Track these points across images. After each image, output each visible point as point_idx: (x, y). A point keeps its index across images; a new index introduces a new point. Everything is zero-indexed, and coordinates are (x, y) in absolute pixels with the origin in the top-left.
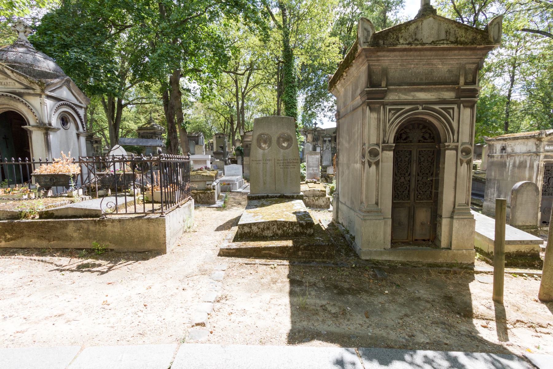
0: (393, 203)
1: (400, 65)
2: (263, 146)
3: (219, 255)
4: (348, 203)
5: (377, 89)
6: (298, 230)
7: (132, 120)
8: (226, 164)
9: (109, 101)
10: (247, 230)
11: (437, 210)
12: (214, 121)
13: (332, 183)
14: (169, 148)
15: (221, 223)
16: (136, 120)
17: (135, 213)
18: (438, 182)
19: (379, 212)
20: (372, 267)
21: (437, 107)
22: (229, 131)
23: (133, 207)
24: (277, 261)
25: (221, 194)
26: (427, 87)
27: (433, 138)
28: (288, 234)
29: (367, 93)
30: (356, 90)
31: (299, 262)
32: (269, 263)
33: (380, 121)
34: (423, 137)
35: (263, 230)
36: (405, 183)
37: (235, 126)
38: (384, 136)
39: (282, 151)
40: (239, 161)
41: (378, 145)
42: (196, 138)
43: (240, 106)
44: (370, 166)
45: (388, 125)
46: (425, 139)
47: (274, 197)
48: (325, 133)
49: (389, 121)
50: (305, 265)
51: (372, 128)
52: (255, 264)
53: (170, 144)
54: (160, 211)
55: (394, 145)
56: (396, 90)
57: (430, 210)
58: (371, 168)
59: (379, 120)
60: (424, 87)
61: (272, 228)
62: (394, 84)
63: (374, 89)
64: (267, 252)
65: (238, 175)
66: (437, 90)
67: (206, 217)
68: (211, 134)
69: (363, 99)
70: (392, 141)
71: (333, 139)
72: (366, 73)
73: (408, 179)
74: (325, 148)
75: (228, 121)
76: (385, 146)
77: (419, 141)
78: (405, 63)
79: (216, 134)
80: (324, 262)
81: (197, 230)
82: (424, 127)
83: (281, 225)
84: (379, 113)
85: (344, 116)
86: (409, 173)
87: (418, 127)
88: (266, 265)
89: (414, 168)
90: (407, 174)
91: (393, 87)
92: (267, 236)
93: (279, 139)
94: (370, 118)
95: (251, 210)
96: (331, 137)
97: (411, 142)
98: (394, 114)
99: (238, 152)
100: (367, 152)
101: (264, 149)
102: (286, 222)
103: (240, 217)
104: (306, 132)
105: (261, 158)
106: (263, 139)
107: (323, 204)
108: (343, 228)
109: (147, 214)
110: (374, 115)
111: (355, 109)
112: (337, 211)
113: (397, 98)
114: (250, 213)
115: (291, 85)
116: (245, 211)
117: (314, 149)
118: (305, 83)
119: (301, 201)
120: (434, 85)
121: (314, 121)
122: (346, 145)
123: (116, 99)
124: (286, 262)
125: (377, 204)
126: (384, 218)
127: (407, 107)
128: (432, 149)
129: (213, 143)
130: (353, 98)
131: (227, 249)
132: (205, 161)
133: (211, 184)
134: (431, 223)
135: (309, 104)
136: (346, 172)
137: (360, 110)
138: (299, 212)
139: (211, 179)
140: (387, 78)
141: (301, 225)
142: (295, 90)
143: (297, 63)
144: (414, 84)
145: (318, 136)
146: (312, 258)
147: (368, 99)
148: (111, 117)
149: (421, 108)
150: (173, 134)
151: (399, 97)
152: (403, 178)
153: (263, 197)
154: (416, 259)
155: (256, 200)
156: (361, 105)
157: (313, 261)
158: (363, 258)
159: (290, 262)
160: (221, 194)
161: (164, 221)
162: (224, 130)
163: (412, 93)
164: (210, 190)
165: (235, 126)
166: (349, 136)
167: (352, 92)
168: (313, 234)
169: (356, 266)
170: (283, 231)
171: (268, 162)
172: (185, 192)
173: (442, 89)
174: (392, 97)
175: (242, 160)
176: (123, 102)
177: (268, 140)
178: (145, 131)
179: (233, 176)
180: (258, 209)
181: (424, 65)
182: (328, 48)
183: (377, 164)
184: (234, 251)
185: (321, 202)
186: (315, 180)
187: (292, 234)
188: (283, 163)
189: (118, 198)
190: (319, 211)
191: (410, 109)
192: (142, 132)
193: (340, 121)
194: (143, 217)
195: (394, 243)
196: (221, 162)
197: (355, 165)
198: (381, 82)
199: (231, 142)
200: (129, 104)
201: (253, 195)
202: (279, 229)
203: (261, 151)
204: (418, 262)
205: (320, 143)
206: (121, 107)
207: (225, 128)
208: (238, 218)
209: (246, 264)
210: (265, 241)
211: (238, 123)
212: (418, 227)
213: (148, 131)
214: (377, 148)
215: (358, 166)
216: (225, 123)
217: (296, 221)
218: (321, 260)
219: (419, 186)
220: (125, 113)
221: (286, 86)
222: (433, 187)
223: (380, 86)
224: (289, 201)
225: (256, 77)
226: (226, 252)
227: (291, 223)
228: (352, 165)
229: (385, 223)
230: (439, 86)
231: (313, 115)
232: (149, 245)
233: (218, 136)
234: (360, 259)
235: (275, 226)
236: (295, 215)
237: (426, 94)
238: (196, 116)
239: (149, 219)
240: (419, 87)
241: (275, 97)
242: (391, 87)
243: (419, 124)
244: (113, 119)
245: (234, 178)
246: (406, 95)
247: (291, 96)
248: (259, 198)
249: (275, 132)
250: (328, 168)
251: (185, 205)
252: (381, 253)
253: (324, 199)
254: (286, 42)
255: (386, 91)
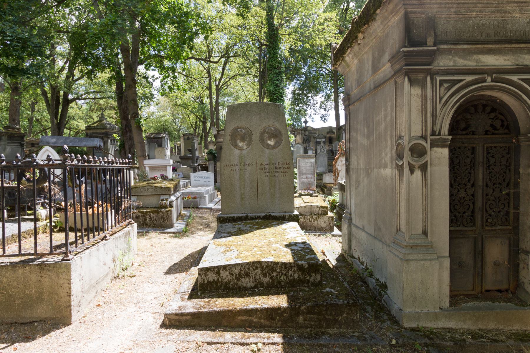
0: (450, 231)
1: (455, 13)
2: (240, 144)
3: (164, 325)
4: (370, 229)
5: (421, 48)
6: (296, 276)
7: (82, 119)
8: (195, 171)
9: (52, 96)
10: (212, 277)
11: (518, 241)
12: (183, 121)
13: (331, 194)
14: (123, 151)
15: (177, 259)
16: (87, 117)
17: (20, 254)
18: (519, 197)
19: (430, 247)
20: (426, 345)
21: (515, 78)
22: (201, 132)
23: (33, 239)
24: (263, 334)
25: (183, 212)
26: (497, 46)
27: (507, 127)
28: (279, 282)
29: (405, 56)
30: (381, 56)
31: (300, 336)
32: (248, 341)
33: (426, 99)
34: (492, 125)
35: (239, 277)
36: (467, 198)
37: (208, 124)
38: (434, 123)
39: (267, 151)
40: (211, 167)
41: (424, 137)
42: (159, 140)
43: (214, 101)
44: (412, 171)
45: (439, 107)
46: (495, 128)
47: (256, 219)
48: (317, 132)
49: (441, 99)
50: (310, 342)
51: (412, 111)
52: (223, 343)
53: (124, 147)
54: (64, 249)
55: (450, 137)
56: (449, 52)
57: (507, 242)
58: (414, 175)
59: (424, 98)
60: (493, 46)
61: (254, 273)
62: (446, 43)
63: (416, 49)
64: (245, 318)
65: (208, 186)
66: (513, 51)
67: (155, 249)
68: (179, 136)
69: (397, 67)
70: (447, 132)
71: (327, 140)
72: (402, 26)
73: (470, 192)
74: (318, 151)
75: (200, 121)
76: (436, 139)
77: (486, 133)
78: (462, 10)
79: (184, 135)
80: (342, 335)
81: (137, 273)
82: (493, 110)
83: (268, 268)
84: (423, 86)
85: (359, 100)
86: (472, 182)
87: (484, 111)
88: (243, 344)
89: (480, 174)
90: (469, 185)
91: (445, 47)
92: (244, 287)
93: (262, 134)
94: (410, 95)
95: (220, 240)
96: (325, 137)
97: (473, 133)
98: (449, 89)
99: (210, 156)
100: (407, 150)
101: (241, 149)
102: (276, 264)
103: (206, 248)
104: (295, 131)
105: (237, 162)
106: (241, 135)
107: (324, 225)
108: (362, 266)
109: (42, 255)
110: (417, 91)
111: (378, 86)
112: (349, 239)
113: (451, 63)
114: (220, 245)
115: (277, 71)
116: (212, 242)
117: (306, 152)
118: (293, 73)
119: (296, 224)
120: (508, 44)
121: (303, 120)
122: (363, 141)
123: (62, 93)
124: (277, 338)
125: (425, 233)
126: (438, 257)
127: (469, 78)
128: (508, 145)
129: (180, 146)
130: (375, 69)
131: (176, 314)
132: (165, 168)
133: (167, 199)
134: (509, 263)
135: (297, 99)
136: (365, 181)
137: (390, 87)
138: (296, 244)
139: (167, 191)
140: (435, 33)
141: (301, 268)
142: (281, 77)
143: (284, 47)
144: (477, 42)
145: (309, 136)
146: (321, 327)
147: (406, 65)
148: (54, 115)
149: (489, 79)
150: (129, 134)
151: (454, 62)
152: (462, 191)
153: (240, 219)
154: (492, 326)
155: (232, 223)
156: (393, 76)
157: (323, 334)
158: (407, 325)
159: (284, 338)
160: (183, 212)
161: (68, 268)
162: (195, 130)
163: (475, 57)
164: (166, 207)
165: (208, 124)
166: (368, 127)
167: (373, 62)
168: (320, 282)
169: (397, 342)
170: (272, 277)
171: (247, 167)
172: (123, 215)
173: (521, 51)
174: (444, 62)
175: (215, 167)
176: (70, 97)
177: (247, 137)
178: (95, 131)
179: (202, 186)
180: (232, 238)
181: (492, 12)
182: (322, 27)
183: (424, 168)
184: (189, 317)
185: (322, 222)
186: (311, 192)
187: (286, 283)
188: (269, 169)
189: (6, 224)
190: (319, 236)
191: (472, 81)
192: (90, 132)
193: (351, 107)
194: (33, 260)
195: (455, 297)
196: (189, 168)
197: (382, 170)
198: (426, 38)
199: (203, 145)
200: (78, 98)
201: (226, 216)
202: (265, 275)
203: (237, 152)
204: (497, 331)
205: (312, 144)
206: (67, 102)
207: (196, 128)
208: (201, 252)
209: (208, 343)
210: (242, 296)
211: (212, 122)
212: (489, 269)
213: (98, 131)
214: (423, 142)
215: (388, 172)
216: (196, 122)
217: (292, 261)
218: (336, 331)
219: (489, 203)
220: (73, 110)
221: (271, 71)
222: (512, 205)
223: (424, 44)
224: (278, 225)
225: (235, 64)
226: (175, 320)
227: (285, 265)
228: (376, 170)
229: (441, 265)
230: (517, 46)
231: (301, 113)
232: (42, 311)
233: (186, 137)
234: (402, 327)
235: (259, 271)
236: (289, 250)
237: (497, 57)
238: (162, 114)
239: (42, 265)
240: (486, 46)
241: (256, 91)
242: (442, 47)
243: (484, 106)
244: (56, 117)
245: (203, 190)
246: (466, 60)
247: (277, 85)
248: (234, 220)
249: (257, 125)
250: (324, 176)
251: (120, 233)
252: (436, 317)
253: (326, 218)
254: (270, 18)
255: (433, 53)
